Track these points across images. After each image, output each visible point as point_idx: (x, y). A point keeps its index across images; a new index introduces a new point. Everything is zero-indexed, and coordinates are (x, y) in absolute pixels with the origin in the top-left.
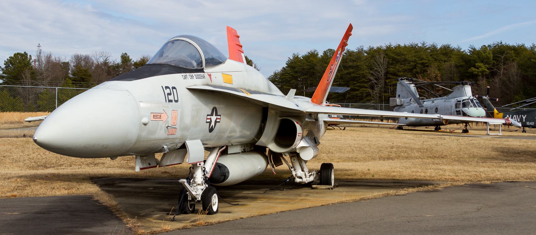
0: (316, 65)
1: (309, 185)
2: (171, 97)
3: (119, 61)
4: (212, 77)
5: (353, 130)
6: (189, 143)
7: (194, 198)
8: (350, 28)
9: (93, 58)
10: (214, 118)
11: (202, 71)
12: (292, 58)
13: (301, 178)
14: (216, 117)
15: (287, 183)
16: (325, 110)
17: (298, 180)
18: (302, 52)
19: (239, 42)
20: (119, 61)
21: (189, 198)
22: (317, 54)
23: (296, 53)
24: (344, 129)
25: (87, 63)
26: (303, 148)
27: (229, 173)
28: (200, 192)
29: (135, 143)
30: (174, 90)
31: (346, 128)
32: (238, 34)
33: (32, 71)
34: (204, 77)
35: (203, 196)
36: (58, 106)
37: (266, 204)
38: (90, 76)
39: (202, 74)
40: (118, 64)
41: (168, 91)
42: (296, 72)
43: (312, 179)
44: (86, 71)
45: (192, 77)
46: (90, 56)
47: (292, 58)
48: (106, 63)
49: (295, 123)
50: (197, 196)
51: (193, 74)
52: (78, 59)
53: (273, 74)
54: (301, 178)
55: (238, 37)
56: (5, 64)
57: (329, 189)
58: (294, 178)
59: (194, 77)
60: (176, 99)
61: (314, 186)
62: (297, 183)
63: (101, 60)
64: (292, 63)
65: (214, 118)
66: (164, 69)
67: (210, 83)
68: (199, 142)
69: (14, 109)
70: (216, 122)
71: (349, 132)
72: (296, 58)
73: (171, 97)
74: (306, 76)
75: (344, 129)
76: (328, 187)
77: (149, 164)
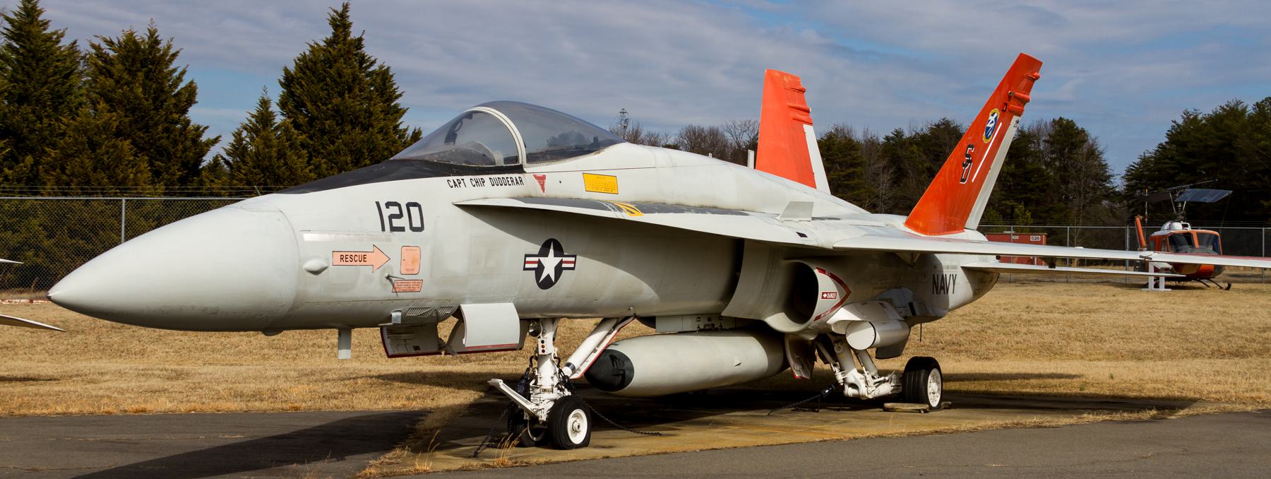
0: (1236, 137)
1: (878, 402)
2: (403, 222)
4: (547, 182)
5: (1251, 291)
6: (467, 309)
9: (728, 136)
10: (550, 262)
11: (520, 169)
12: (1180, 121)
13: (854, 386)
14: (559, 259)
15: (831, 398)
16: (963, 249)
17: (850, 391)
18: (1207, 107)
19: (804, 102)
21: (526, 417)
22: (1244, 110)
23: (1191, 110)
24: (1228, 288)
26: (851, 325)
27: (632, 370)
29: (291, 309)
30: (414, 210)
31: (1233, 285)
32: (803, 86)
35: (552, 412)
36: (127, 239)
39: (517, 176)
41: (395, 210)
42: (1189, 155)
43: (886, 389)
46: (721, 130)
47: (1180, 121)
49: (816, 271)
50: (539, 413)
51: (486, 177)
53: (1138, 161)
54: (854, 386)
55: (802, 91)
57: (919, 411)
60: (417, 224)
61: (888, 405)
64: (1180, 133)
65: (550, 262)
66: (404, 170)
67: (539, 192)
70: (559, 270)
71: (1243, 297)
72: (1191, 121)
73: (396, 223)
74: (1213, 164)
75: (1228, 288)
76: (918, 407)
77: (416, 348)
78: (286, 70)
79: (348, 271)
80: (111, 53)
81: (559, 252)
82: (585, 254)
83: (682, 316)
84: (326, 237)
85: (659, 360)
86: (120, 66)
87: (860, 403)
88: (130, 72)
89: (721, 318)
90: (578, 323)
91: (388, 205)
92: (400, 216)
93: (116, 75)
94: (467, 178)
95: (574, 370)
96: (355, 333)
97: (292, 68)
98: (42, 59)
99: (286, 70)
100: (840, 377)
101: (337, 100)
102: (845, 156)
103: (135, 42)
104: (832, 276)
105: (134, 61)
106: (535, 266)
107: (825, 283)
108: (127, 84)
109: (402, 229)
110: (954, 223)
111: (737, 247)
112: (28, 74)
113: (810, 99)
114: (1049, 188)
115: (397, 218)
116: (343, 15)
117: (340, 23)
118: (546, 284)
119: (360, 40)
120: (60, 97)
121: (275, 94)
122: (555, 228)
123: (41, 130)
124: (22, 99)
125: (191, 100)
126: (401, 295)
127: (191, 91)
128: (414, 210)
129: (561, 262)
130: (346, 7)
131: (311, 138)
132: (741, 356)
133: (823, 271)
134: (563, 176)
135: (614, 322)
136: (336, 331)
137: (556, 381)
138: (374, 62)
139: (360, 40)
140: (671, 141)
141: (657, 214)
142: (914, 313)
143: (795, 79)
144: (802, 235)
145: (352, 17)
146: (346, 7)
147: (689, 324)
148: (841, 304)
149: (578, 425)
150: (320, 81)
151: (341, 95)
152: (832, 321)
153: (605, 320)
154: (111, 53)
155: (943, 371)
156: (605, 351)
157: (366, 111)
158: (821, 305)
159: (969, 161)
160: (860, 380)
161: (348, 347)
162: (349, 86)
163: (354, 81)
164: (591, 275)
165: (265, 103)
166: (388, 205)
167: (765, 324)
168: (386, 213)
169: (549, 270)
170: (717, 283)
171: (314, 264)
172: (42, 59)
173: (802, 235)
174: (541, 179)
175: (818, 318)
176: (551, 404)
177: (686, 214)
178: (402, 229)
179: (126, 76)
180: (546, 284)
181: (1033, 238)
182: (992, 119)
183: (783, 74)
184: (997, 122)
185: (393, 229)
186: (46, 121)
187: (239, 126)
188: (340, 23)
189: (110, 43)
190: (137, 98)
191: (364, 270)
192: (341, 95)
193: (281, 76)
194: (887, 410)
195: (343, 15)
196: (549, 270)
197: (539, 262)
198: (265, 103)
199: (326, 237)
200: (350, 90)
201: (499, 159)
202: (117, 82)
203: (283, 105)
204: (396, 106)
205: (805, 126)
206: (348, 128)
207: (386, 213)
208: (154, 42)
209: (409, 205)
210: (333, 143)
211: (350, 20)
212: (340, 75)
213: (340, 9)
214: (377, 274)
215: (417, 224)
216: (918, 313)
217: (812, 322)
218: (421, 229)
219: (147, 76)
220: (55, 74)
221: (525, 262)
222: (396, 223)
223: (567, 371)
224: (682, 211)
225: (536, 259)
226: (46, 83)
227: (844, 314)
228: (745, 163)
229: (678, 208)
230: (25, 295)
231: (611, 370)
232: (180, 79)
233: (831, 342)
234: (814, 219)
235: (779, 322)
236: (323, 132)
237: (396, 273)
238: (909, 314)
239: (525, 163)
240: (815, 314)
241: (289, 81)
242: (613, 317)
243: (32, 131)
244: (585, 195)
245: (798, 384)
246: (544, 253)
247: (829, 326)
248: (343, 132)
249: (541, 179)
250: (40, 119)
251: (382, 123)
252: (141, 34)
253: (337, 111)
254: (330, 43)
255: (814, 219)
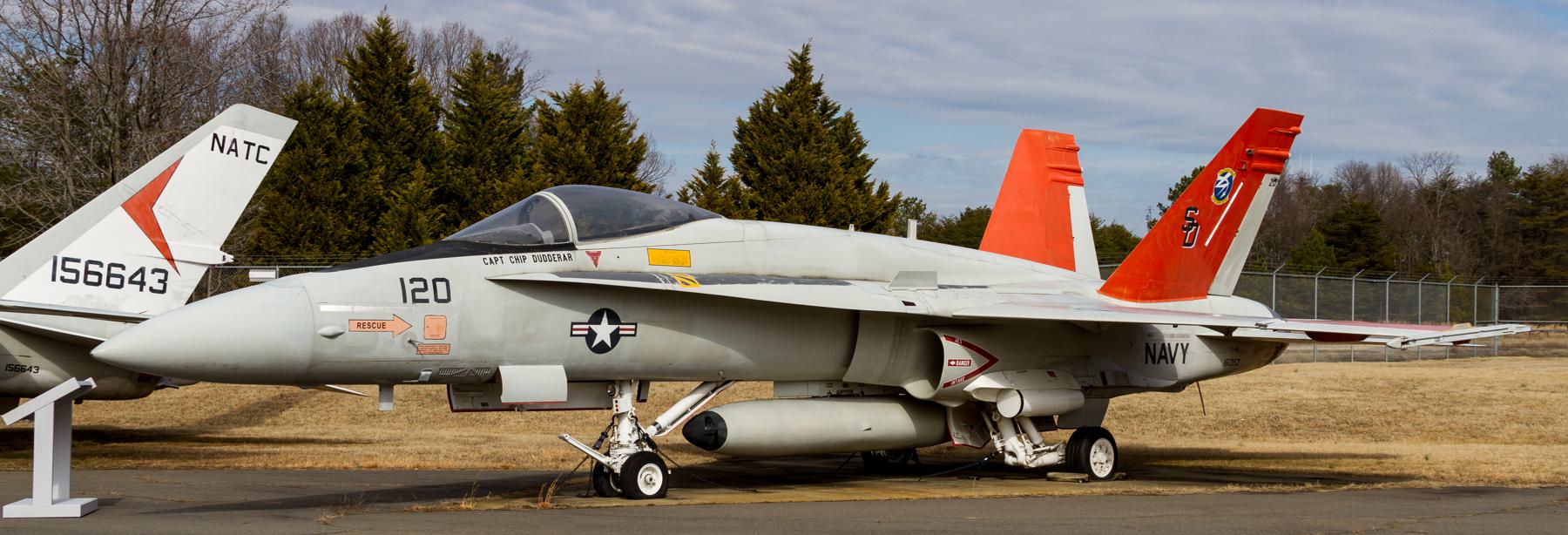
1: (1041, 473)
3: (1483, 174)
4: (601, 259)
11: (571, 247)
13: (1013, 454)
14: (614, 327)
17: (1009, 460)
20: (1483, 174)
26: (1001, 392)
27: (725, 430)
28: (621, 461)
35: (625, 467)
38: (1377, 220)
40: (1484, 185)
41: (420, 285)
44: (1365, 208)
48: (1445, 183)
49: (943, 339)
54: (1013, 454)
56: (1170, 198)
58: (1003, 457)
61: (1050, 474)
62: (1008, 466)
63: (1429, 177)
65: (604, 331)
67: (590, 266)
68: (561, 368)
69: (1099, 324)
70: (615, 337)
73: (419, 295)
76: (1077, 476)
78: (740, 121)
79: (365, 337)
80: (558, 109)
81: (614, 319)
82: (645, 322)
83: (808, 382)
84: (371, 308)
85: (755, 421)
86: (565, 123)
87: (1020, 472)
88: (574, 128)
90: (678, 385)
91: (412, 281)
93: (561, 132)
94: (506, 257)
95: (660, 430)
96: (398, 389)
97: (746, 117)
98: (488, 117)
99: (740, 121)
100: (998, 445)
101: (790, 153)
102: (1556, 196)
103: (580, 96)
104: (964, 344)
105: (578, 118)
108: (570, 142)
109: (426, 301)
111: (854, 319)
112: (474, 135)
113: (1084, 161)
114: (1353, 246)
115: (415, 293)
116: (803, 58)
117: (801, 66)
118: (602, 348)
119: (820, 84)
120: (507, 157)
121: (726, 147)
122: (609, 300)
123: (484, 192)
124: (468, 161)
125: (637, 159)
126: (427, 357)
127: (640, 148)
128: (441, 286)
130: (806, 49)
131: (762, 194)
132: (886, 421)
133: (949, 338)
134: (618, 252)
135: (713, 386)
136: (377, 387)
137: (635, 437)
138: (836, 110)
139: (820, 84)
140: (946, 208)
142: (1105, 382)
143: (1069, 139)
144: (907, 304)
145: (814, 60)
146: (806, 49)
147: (815, 390)
148: (981, 371)
149: (651, 480)
150: (773, 132)
151: (796, 147)
153: (705, 383)
154: (558, 109)
155: (1119, 441)
157: (823, 164)
160: (1018, 449)
161: (390, 399)
162: (803, 137)
163: (810, 131)
164: (652, 340)
165: (713, 159)
167: (904, 391)
170: (835, 351)
171: (329, 330)
172: (488, 117)
173: (907, 304)
174: (595, 256)
177: (758, 286)
178: (426, 301)
179: (570, 133)
183: (1046, 134)
185: (415, 301)
186: (488, 182)
187: (684, 184)
188: (801, 66)
189: (557, 98)
190: (579, 156)
191: (383, 336)
192: (796, 147)
193: (735, 127)
194: (1050, 479)
195: (803, 58)
197: (590, 330)
198: (713, 159)
199: (371, 308)
200: (806, 142)
201: (547, 236)
202: (561, 140)
203: (735, 159)
204: (864, 157)
205: (1071, 188)
206: (803, 183)
207: (409, 287)
208: (600, 92)
209: (435, 281)
210: (785, 200)
211: (811, 63)
212: (795, 126)
213: (800, 51)
214: (398, 339)
215: (442, 295)
216: (1111, 383)
218: (448, 300)
219: (592, 133)
220: (501, 133)
223: (651, 431)
224: (754, 282)
226: (491, 143)
227: (983, 381)
228: (904, 234)
229: (751, 279)
231: (704, 431)
232: (629, 134)
233: (979, 414)
234: (941, 287)
235: (919, 388)
236: (776, 189)
237: (419, 338)
239: (576, 241)
241: (743, 132)
242: (715, 379)
243: (475, 195)
244: (647, 269)
245: (953, 447)
246: (596, 319)
248: (797, 188)
250: (484, 180)
251: (842, 177)
252: (588, 87)
253: (790, 165)
254: (790, 88)
255: (941, 287)
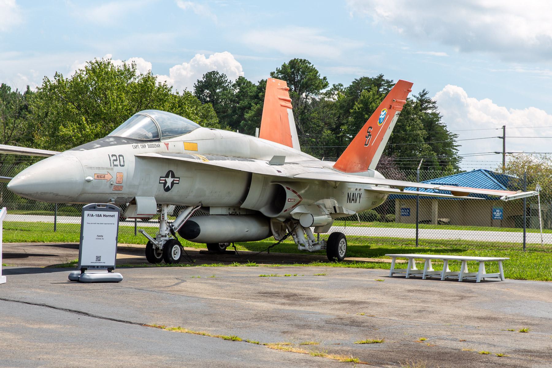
2: (117, 163)
4: (169, 146)
6: (139, 200)
7: (157, 249)
8: (282, 106)
10: (169, 180)
25: (193, 262)
30: (121, 158)
33: (167, 104)
34: (159, 146)
37: (274, 265)
41: (114, 158)
45: (144, 147)
51: (146, 144)
52: (321, 159)
59: (147, 146)
60: (122, 164)
65: (169, 180)
67: (167, 151)
70: (173, 184)
73: (116, 163)
81: (173, 176)
89: (240, 209)
91: (113, 156)
92: (117, 160)
106: (164, 182)
107: (289, 194)
110: (365, 167)
111: (250, 176)
128: (121, 158)
129: (174, 180)
141: (221, 161)
152: (292, 213)
156: (187, 221)
158: (288, 205)
159: (369, 135)
166: (113, 156)
168: (112, 159)
169: (169, 184)
173: (279, 172)
174: (167, 145)
175: (286, 211)
176: (165, 242)
180: (167, 189)
181: (59, 147)
182: (382, 113)
184: (386, 115)
196: (169, 184)
197: (165, 180)
209: (119, 156)
217: (282, 213)
218: (123, 166)
221: (160, 180)
222: (116, 163)
225: (164, 179)
230: (427, 347)
238: (333, 212)
240: (285, 209)
241: (400, 81)
246: (167, 176)
247: (291, 215)
249: (167, 145)
